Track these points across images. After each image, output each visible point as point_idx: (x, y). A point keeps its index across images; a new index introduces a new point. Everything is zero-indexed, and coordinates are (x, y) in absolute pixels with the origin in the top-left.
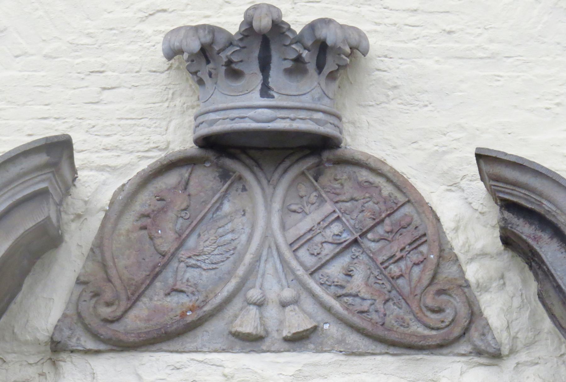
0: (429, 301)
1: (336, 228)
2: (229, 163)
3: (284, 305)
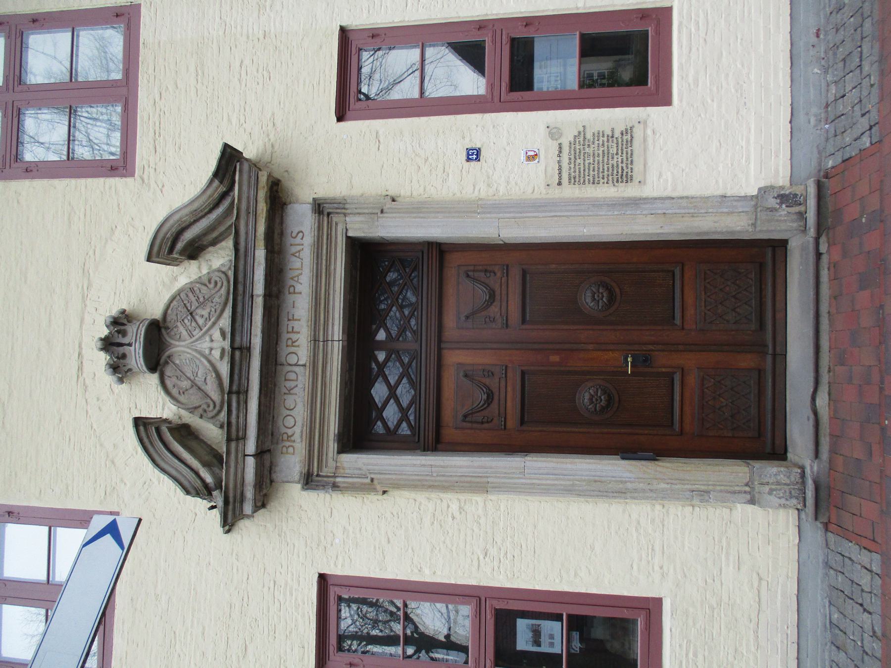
0: (212, 286)
1: (186, 321)
2: (162, 361)
3: (212, 341)
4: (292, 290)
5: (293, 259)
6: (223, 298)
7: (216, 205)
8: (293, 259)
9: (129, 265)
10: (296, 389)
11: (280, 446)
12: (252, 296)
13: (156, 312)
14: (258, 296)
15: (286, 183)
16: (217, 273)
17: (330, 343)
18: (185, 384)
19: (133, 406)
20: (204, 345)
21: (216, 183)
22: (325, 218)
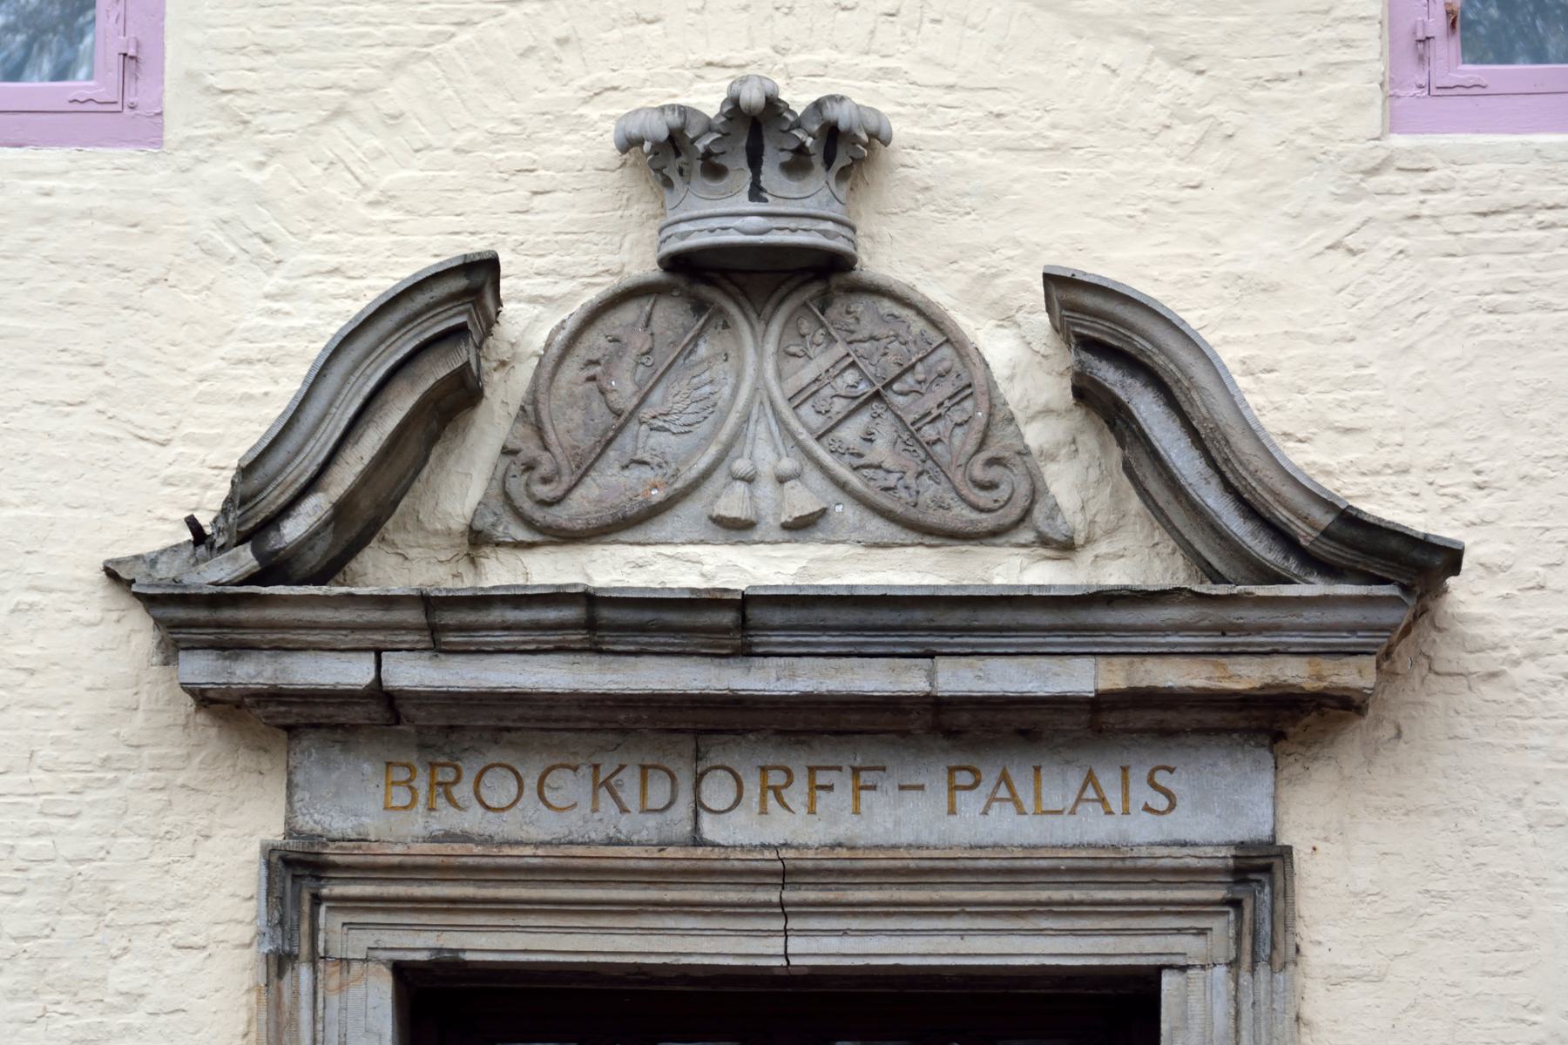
0: (978, 472)
1: (850, 377)
2: (704, 291)
3: (782, 480)
4: (964, 778)
5: (1075, 779)
6: (934, 518)
7: (1250, 510)
8: (1075, 779)
9: (1057, 135)
10: (614, 809)
11: (413, 758)
12: (931, 655)
13: (886, 256)
14: (931, 676)
15: (1351, 743)
16: (1023, 489)
17: (778, 924)
18: (624, 388)
19: (545, 177)
20: (764, 453)
21: (1325, 519)
22: (1220, 894)
